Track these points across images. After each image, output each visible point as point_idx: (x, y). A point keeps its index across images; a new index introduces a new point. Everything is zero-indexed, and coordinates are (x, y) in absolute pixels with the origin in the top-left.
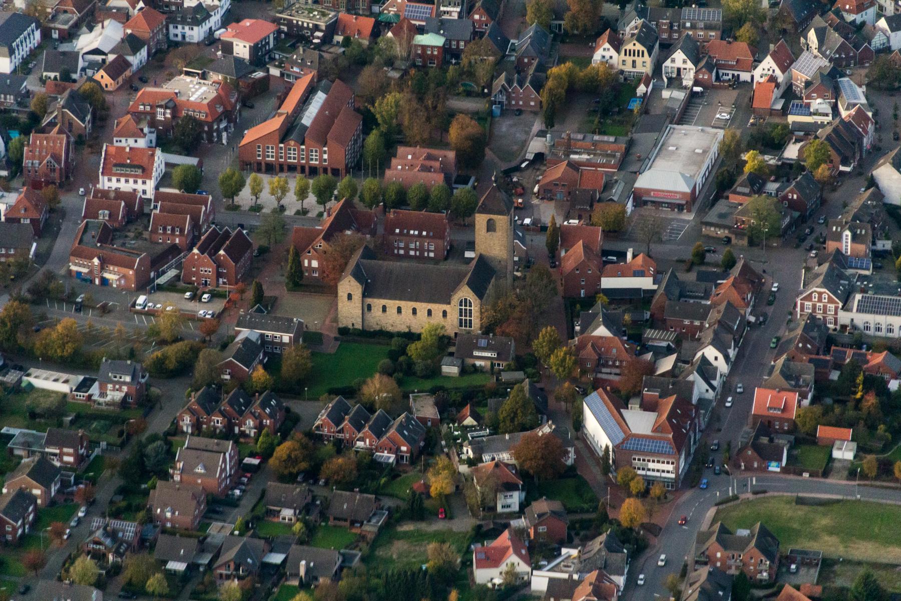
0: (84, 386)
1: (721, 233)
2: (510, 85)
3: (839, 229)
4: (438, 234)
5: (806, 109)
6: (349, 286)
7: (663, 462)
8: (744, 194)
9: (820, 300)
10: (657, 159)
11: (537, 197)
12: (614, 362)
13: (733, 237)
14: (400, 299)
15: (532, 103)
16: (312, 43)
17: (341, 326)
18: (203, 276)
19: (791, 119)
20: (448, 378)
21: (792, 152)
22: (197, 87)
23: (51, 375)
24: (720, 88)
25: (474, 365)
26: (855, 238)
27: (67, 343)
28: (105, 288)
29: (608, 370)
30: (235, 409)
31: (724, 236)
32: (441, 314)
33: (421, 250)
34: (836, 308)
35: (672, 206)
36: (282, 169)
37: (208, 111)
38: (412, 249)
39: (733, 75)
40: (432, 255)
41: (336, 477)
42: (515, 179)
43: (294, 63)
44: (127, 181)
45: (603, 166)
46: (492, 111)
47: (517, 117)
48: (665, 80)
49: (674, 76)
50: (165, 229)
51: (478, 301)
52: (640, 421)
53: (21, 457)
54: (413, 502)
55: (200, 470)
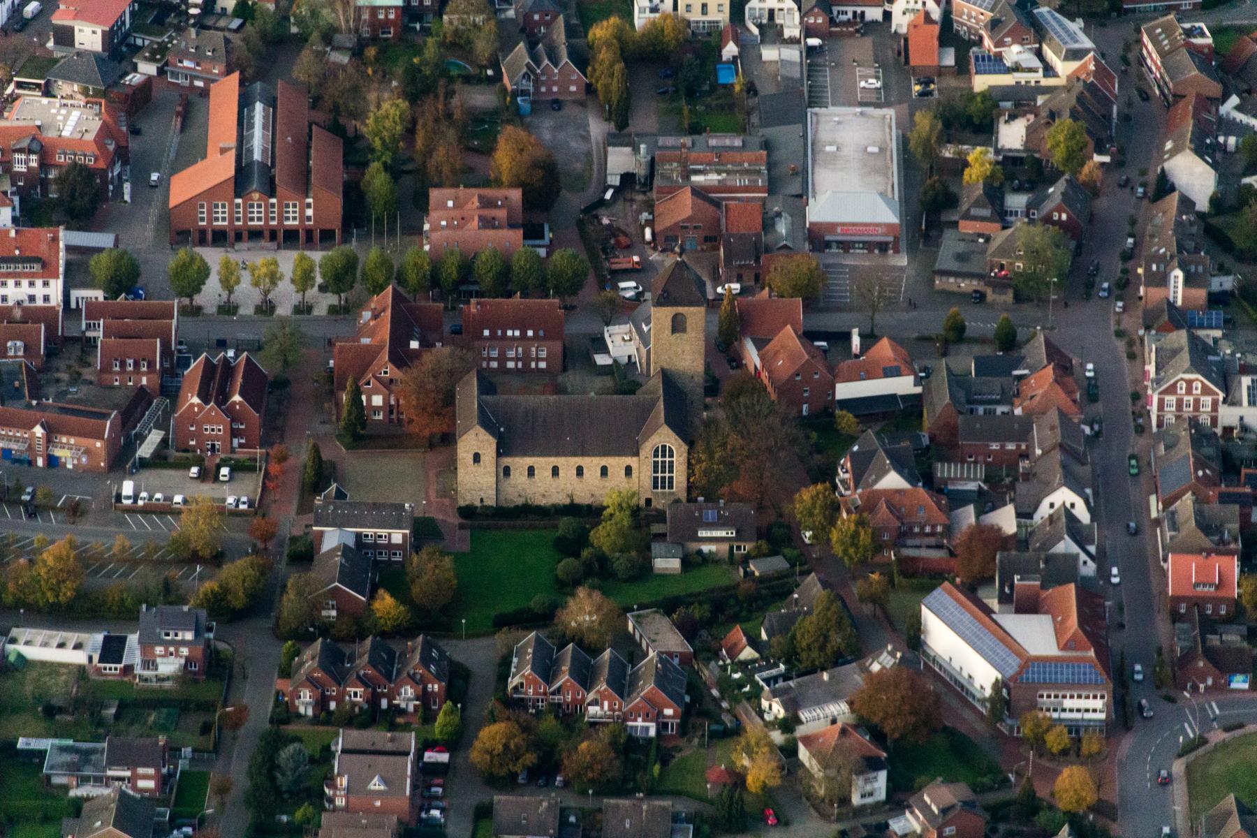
0: (112, 649)
1: (965, 285)
2: (538, 63)
3: (1162, 267)
4: (550, 332)
5: (996, 64)
6: (475, 442)
7: (1087, 697)
8: (983, 219)
9: (1189, 391)
10: (816, 170)
11: (655, 249)
12: (922, 528)
13: (989, 291)
14: (557, 455)
15: (573, 88)
16: (189, 16)
17: (462, 503)
18: (210, 438)
19: (981, 82)
20: (665, 577)
21: (1012, 135)
22: (63, 111)
23: (51, 637)
24: (841, 35)
25: (700, 552)
26: (1188, 281)
27: (64, 581)
28: (54, 471)
29: (917, 542)
30: (380, 672)
31: (970, 290)
32: (623, 472)
33: (526, 359)
34: (1215, 404)
35: (869, 246)
36: (238, 237)
37: (97, 152)
38: (511, 359)
39: (855, 13)
40: (543, 365)
41: (590, 775)
42: (605, 221)
43: (184, 55)
44: (17, 284)
45: (746, 189)
46: (518, 107)
47: (557, 114)
48: (756, 31)
49: (765, 21)
50: (123, 364)
51: (685, 448)
52: (1037, 636)
53: (66, 788)
54: (730, 806)
55: (376, 785)
